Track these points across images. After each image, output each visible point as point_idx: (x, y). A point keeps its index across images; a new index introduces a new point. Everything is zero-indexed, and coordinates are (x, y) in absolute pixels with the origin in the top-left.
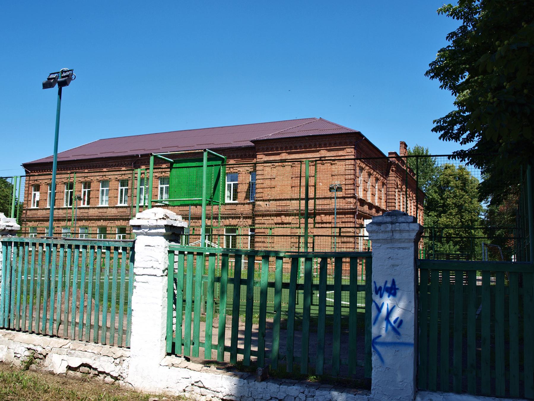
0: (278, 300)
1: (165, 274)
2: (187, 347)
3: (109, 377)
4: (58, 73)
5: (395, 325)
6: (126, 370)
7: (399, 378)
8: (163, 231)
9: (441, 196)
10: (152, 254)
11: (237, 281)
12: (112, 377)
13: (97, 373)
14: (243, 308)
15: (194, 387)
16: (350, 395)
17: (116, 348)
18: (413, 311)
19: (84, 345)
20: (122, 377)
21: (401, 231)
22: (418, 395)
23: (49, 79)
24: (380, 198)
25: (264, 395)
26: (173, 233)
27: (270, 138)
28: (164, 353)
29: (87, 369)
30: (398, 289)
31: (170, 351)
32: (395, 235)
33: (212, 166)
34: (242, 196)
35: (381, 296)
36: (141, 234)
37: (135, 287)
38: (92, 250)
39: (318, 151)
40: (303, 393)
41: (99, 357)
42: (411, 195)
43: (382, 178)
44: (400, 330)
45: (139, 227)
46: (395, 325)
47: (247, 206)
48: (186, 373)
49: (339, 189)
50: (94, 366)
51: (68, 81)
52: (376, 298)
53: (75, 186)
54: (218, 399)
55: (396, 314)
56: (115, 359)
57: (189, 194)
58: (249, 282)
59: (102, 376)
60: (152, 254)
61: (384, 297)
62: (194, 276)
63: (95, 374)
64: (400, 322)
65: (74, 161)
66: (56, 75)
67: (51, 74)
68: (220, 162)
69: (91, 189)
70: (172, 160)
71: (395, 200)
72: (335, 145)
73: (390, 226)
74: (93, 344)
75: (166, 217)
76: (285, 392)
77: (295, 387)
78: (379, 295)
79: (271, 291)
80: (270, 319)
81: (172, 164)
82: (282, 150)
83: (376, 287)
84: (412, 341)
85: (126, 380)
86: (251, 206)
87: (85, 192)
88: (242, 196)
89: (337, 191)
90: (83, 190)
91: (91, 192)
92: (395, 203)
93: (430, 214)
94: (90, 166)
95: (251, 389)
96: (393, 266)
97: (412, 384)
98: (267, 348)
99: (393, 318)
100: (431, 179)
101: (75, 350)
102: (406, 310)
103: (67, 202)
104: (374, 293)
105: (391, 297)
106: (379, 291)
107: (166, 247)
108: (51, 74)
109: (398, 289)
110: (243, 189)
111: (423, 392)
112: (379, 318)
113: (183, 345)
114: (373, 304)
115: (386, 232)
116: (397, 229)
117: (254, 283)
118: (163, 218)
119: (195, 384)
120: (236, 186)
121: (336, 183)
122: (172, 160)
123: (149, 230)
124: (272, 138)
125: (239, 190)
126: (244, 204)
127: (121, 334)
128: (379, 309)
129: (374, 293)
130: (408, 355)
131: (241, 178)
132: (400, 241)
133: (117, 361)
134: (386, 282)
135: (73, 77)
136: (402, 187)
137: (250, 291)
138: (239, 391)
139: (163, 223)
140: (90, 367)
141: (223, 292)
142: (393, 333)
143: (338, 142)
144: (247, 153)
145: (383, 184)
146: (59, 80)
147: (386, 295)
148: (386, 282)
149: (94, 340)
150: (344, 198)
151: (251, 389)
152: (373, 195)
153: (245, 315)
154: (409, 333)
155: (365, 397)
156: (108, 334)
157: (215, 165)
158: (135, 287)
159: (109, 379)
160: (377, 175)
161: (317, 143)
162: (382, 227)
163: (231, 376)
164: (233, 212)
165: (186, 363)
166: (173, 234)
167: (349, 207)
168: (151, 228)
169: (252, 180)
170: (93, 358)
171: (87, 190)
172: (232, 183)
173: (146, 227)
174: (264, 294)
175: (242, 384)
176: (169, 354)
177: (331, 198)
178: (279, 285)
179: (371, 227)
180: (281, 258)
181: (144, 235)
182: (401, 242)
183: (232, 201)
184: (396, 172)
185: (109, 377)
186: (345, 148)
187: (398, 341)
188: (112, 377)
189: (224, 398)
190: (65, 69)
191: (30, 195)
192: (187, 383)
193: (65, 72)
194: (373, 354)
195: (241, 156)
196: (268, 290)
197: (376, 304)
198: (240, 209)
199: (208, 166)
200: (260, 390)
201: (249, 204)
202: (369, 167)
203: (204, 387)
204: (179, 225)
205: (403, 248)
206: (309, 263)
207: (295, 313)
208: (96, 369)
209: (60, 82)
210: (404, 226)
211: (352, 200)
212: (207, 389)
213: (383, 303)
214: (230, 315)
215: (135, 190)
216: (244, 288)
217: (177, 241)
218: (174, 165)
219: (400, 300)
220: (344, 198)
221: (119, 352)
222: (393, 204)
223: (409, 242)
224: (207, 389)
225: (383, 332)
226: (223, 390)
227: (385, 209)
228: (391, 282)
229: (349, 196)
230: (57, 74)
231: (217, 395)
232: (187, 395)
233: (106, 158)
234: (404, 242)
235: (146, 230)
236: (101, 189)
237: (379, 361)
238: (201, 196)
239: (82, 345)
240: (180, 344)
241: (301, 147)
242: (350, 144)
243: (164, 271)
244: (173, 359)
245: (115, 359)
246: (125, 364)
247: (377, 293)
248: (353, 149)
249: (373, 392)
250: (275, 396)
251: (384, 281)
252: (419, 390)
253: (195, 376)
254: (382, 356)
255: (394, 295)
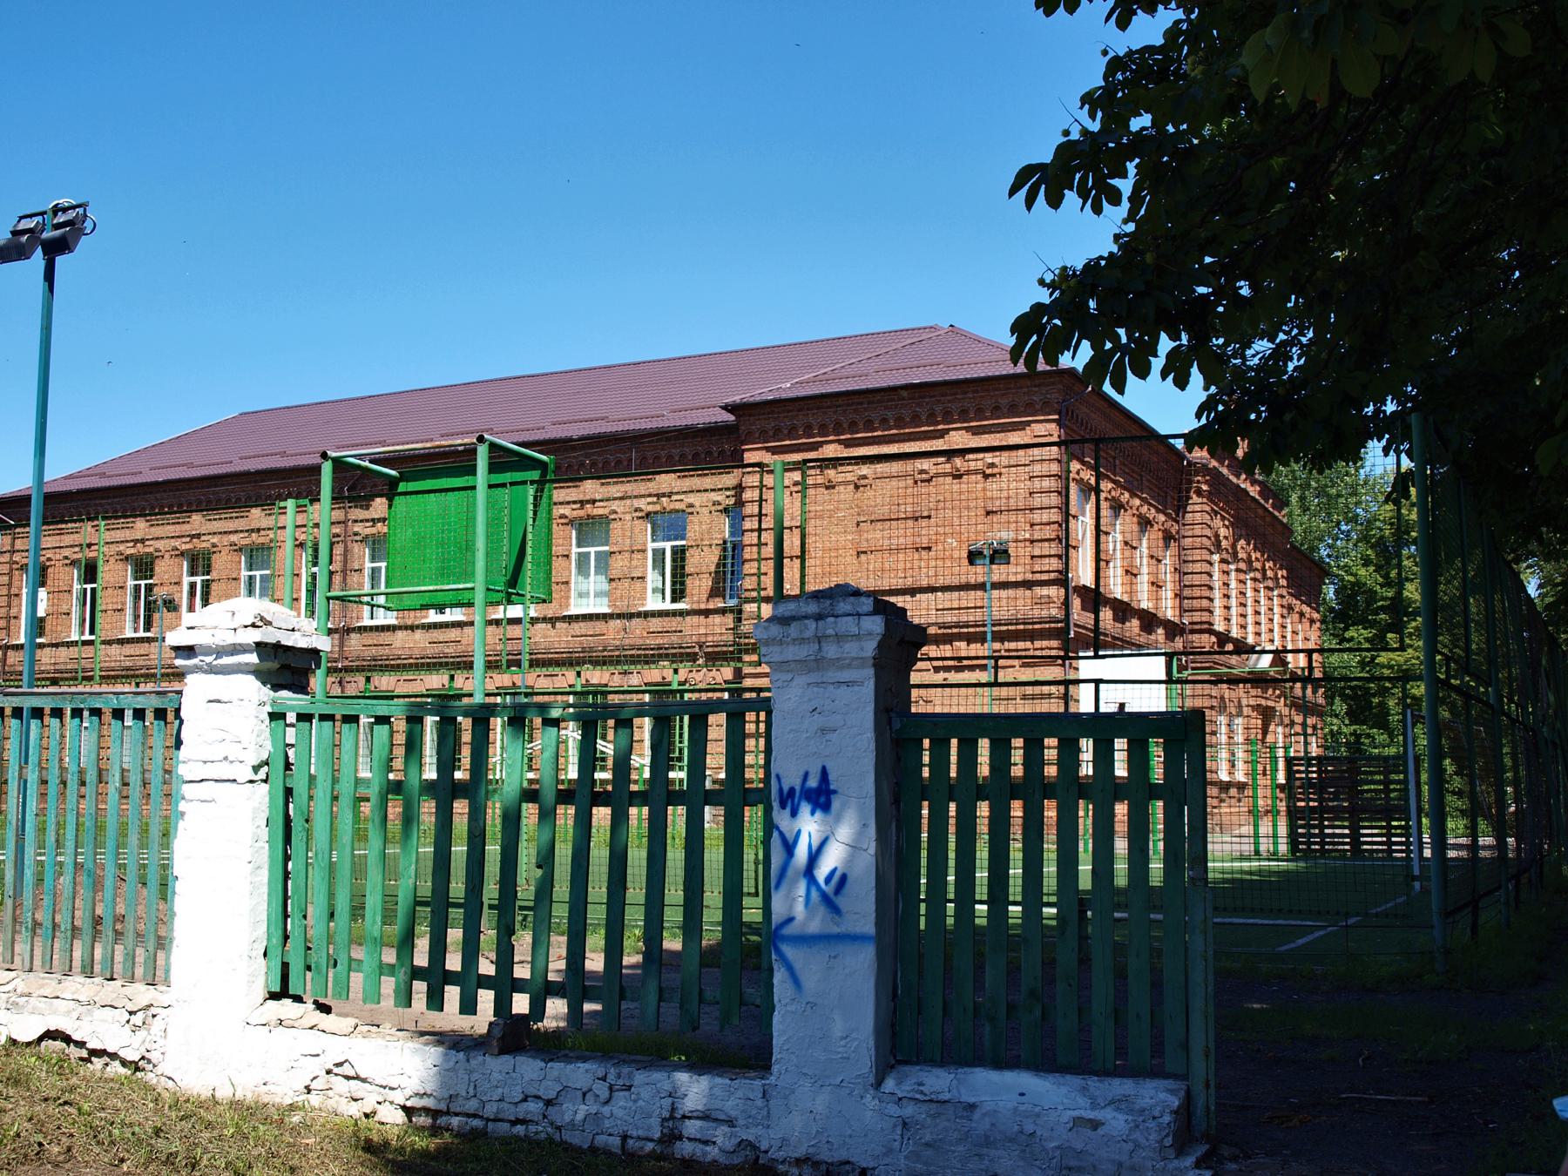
0: (546, 836)
1: (262, 774)
2: (319, 973)
3: (117, 1063)
4: (42, 214)
5: (829, 889)
6: (161, 1042)
7: (838, 1028)
8: (253, 658)
9: (1386, 577)
10: (226, 719)
11: (445, 791)
12: (124, 1063)
13: (85, 1054)
14: (597, 913)
15: (332, 1078)
16: (719, 1080)
17: (140, 987)
18: (872, 850)
19: (54, 983)
20: (149, 1061)
21: (839, 638)
22: (893, 1075)
23: (16, 233)
24: (1156, 585)
25: (506, 1091)
26: (284, 667)
27: (784, 396)
28: (261, 993)
29: (59, 1045)
30: (835, 792)
31: (276, 988)
32: (825, 647)
33: (503, 485)
34: (699, 587)
35: (794, 814)
36: (197, 669)
37: (183, 814)
38: (77, 720)
39: (941, 434)
40: (604, 1079)
41: (92, 1012)
42: (1270, 573)
43: (1162, 518)
44: (840, 901)
45: (188, 651)
46: (829, 889)
47: (717, 619)
48: (314, 1041)
49: (1000, 555)
50: (76, 1037)
51: (70, 240)
52: (782, 818)
53: (161, 568)
54: (392, 1108)
55: (831, 860)
56: (131, 1013)
57: (444, 574)
58: (477, 788)
59: (98, 1063)
60: (226, 719)
61: (800, 814)
62: (335, 781)
63: (82, 1059)
64: (841, 881)
65: (156, 484)
66: (36, 219)
67: (21, 218)
68: (535, 475)
69: (214, 575)
70: (393, 473)
71: (1211, 588)
72: (997, 411)
73: (812, 624)
74: (81, 979)
75: (263, 622)
76: (558, 1080)
77: (583, 1066)
78: (788, 810)
79: (530, 811)
80: (672, 943)
81: (393, 483)
82: (823, 431)
83: (781, 790)
84: (869, 928)
85: (159, 1070)
86: (729, 620)
87: (193, 586)
88: (699, 587)
89: (992, 562)
90: (186, 580)
91: (214, 586)
92: (1211, 600)
93: (1348, 635)
94: (209, 502)
95: (475, 1076)
96: (823, 731)
97: (872, 1043)
98: (592, 1000)
99: (822, 873)
100: (1354, 519)
101: (29, 995)
102: (854, 848)
103: (137, 617)
104: (776, 805)
105: (818, 814)
106: (789, 800)
107: (262, 704)
108: (21, 218)
109: (835, 792)
110: (703, 562)
111: (906, 1068)
112: (790, 873)
113: (309, 968)
114: (775, 834)
115: (802, 641)
116: (830, 632)
117: (487, 792)
118: (253, 625)
119: (336, 1070)
120: (679, 555)
121: (1002, 533)
122: (393, 473)
123: (219, 659)
124: (791, 395)
125: (688, 569)
126: (706, 613)
127: (151, 949)
128: (789, 848)
129: (776, 805)
130: (861, 965)
131: (695, 529)
132: (838, 664)
133: (137, 1019)
134: (806, 775)
135: (88, 225)
136: (1234, 546)
137: (477, 816)
138: (443, 1084)
139: (254, 636)
140: (67, 1039)
141: (409, 819)
142: (822, 910)
143: (1004, 402)
144: (710, 446)
145: (1168, 537)
146: (45, 235)
147: (805, 809)
148: (806, 775)
149: (83, 967)
150: (1028, 585)
151: (475, 1076)
152: (1131, 573)
153: (603, 932)
154: (862, 912)
155: (758, 1083)
156: (119, 949)
157: (512, 484)
158: (183, 814)
159: (116, 1068)
160: (1144, 509)
161: (938, 409)
162: (793, 630)
163: (426, 1044)
164: (675, 639)
165: (319, 1017)
166: (285, 667)
167: (1045, 613)
168: (220, 652)
169: (732, 534)
170: (75, 1015)
171: (198, 579)
172: (668, 546)
173: (207, 651)
174: (512, 821)
175: (452, 1064)
176: (274, 996)
177: (981, 587)
178: (549, 795)
179: (766, 628)
180: (556, 723)
181: (206, 672)
182: (842, 668)
183: (668, 605)
184: (1211, 496)
185: (117, 1063)
186: (1029, 423)
187: (836, 930)
188: (124, 1063)
189: (409, 1104)
190: (64, 201)
191: (15, 601)
192: (317, 1067)
193: (65, 210)
194: (775, 967)
195: (696, 455)
196: (524, 813)
197: (781, 833)
198: (694, 629)
199: (490, 486)
200: (496, 1075)
201: (723, 611)
202: (1114, 482)
203: (357, 1078)
204: (302, 643)
205: (848, 684)
206: (623, 732)
207: (742, 924)
208: (81, 1044)
209: (54, 238)
210: (848, 625)
211: (1053, 591)
212: (364, 1080)
213: (799, 832)
214: (562, 934)
215: (356, 575)
216: (461, 807)
217: (301, 688)
218: (402, 487)
219: (838, 819)
220: (1028, 585)
221: (141, 994)
222: (1205, 603)
223: (862, 666)
224: (364, 1080)
225: (799, 909)
226: (404, 1082)
227: (1177, 620)
228: (818, 775)
229: (1045, 577)
230: (40, 219)
231: (392, 1095)
232: (315, 1100)
233: (258, 472)
234: (849, 666)
235: (209, 659)
236: (244, 573)
237: (789, 985)
238: (468, 575)
239: (50, 985)
240: (301, 966)
241: (884, 423)
242: (1045, 408)
243: (256, 769)
244: (286, 1007)
245: (131, 1013)
246: (157, 1025)
247: (783, 806)
248: (1054, 425)
249: (775, 1068)
250: (535, 1092)
251: (802, 773)
252: (899, 1062)
253: (335, 1049)
254: (798, 973)
255: (826, 808)
